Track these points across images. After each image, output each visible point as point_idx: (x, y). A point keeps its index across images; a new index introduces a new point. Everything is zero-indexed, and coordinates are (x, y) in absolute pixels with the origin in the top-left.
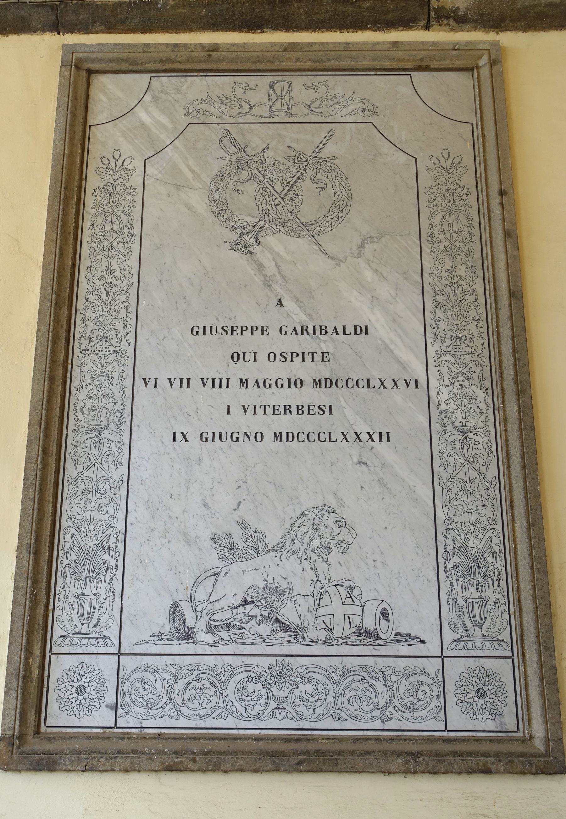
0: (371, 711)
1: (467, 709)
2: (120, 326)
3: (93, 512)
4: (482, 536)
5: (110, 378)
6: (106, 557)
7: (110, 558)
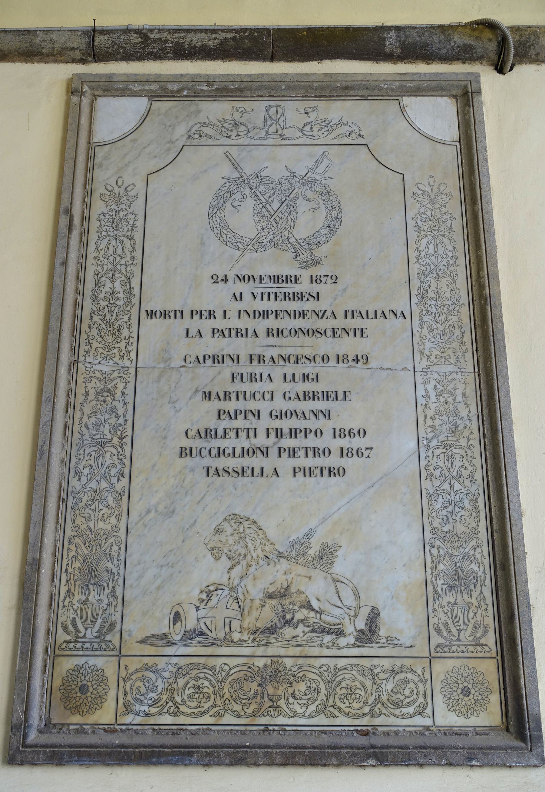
0: (361, 708)
1: (453, 706)
2: (122, 345)
3: (96, 521)
4: (467, 544)
5: (113, 394)
6: (110, 565)
7: (113, 566)
